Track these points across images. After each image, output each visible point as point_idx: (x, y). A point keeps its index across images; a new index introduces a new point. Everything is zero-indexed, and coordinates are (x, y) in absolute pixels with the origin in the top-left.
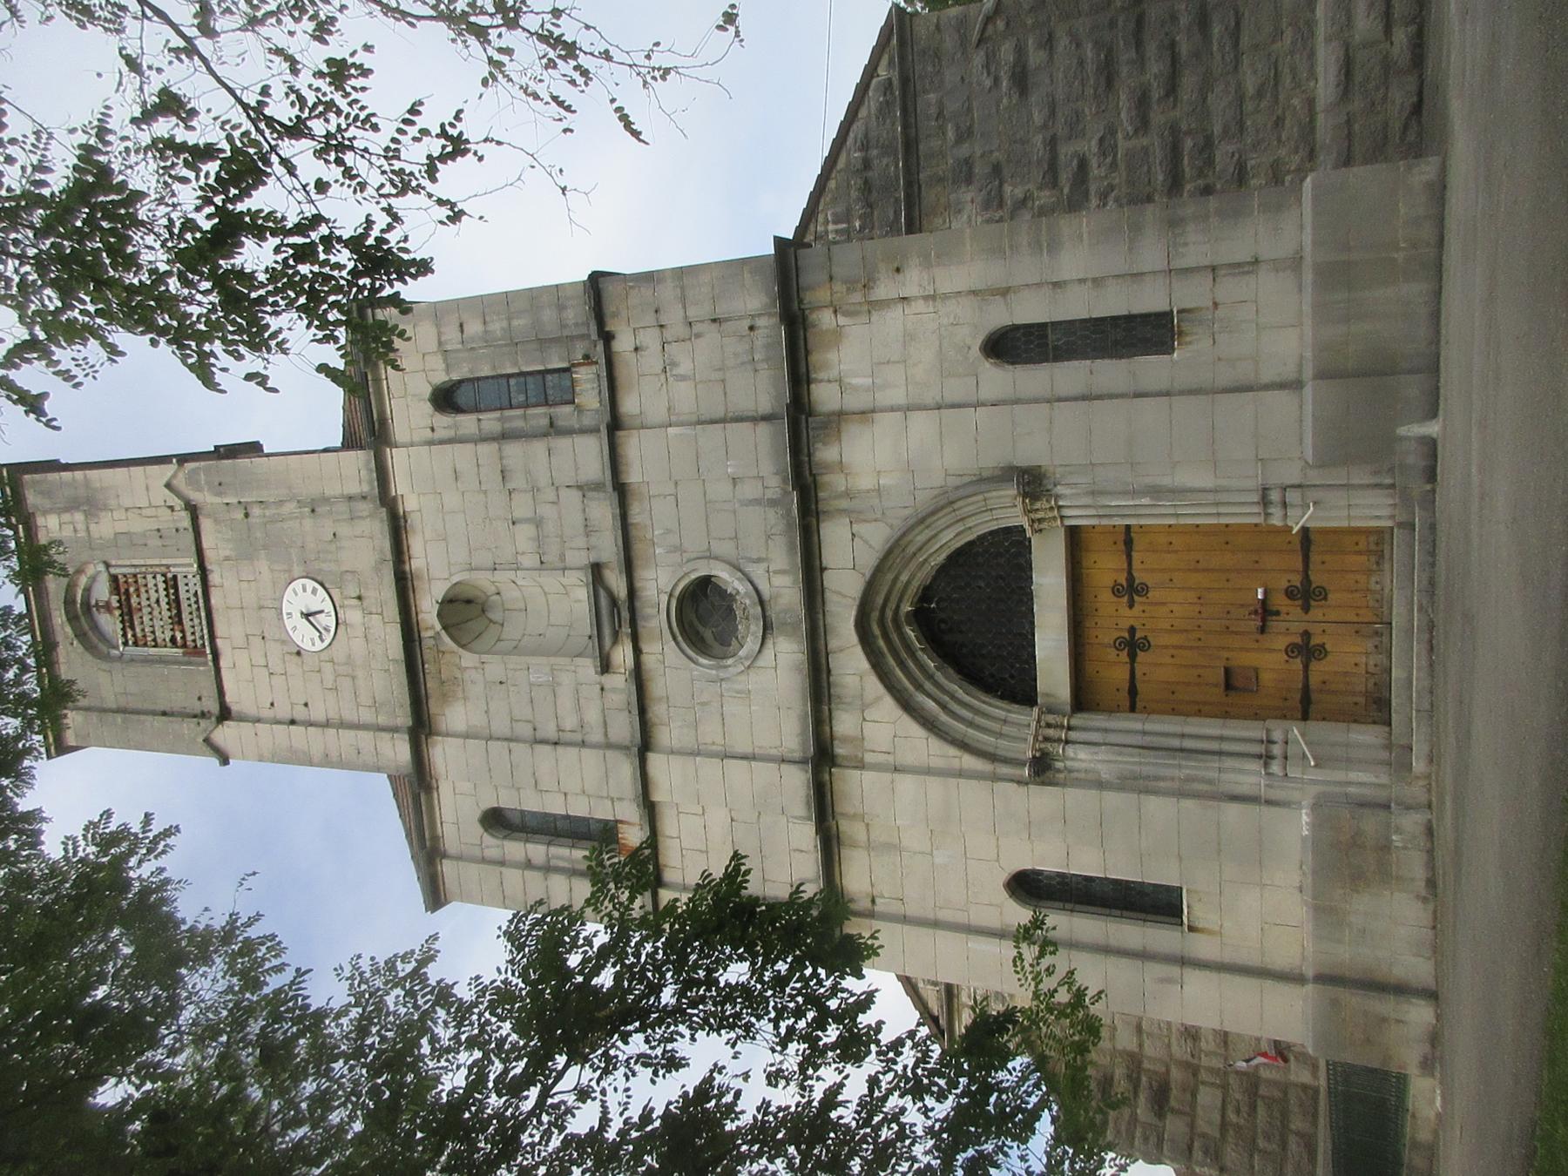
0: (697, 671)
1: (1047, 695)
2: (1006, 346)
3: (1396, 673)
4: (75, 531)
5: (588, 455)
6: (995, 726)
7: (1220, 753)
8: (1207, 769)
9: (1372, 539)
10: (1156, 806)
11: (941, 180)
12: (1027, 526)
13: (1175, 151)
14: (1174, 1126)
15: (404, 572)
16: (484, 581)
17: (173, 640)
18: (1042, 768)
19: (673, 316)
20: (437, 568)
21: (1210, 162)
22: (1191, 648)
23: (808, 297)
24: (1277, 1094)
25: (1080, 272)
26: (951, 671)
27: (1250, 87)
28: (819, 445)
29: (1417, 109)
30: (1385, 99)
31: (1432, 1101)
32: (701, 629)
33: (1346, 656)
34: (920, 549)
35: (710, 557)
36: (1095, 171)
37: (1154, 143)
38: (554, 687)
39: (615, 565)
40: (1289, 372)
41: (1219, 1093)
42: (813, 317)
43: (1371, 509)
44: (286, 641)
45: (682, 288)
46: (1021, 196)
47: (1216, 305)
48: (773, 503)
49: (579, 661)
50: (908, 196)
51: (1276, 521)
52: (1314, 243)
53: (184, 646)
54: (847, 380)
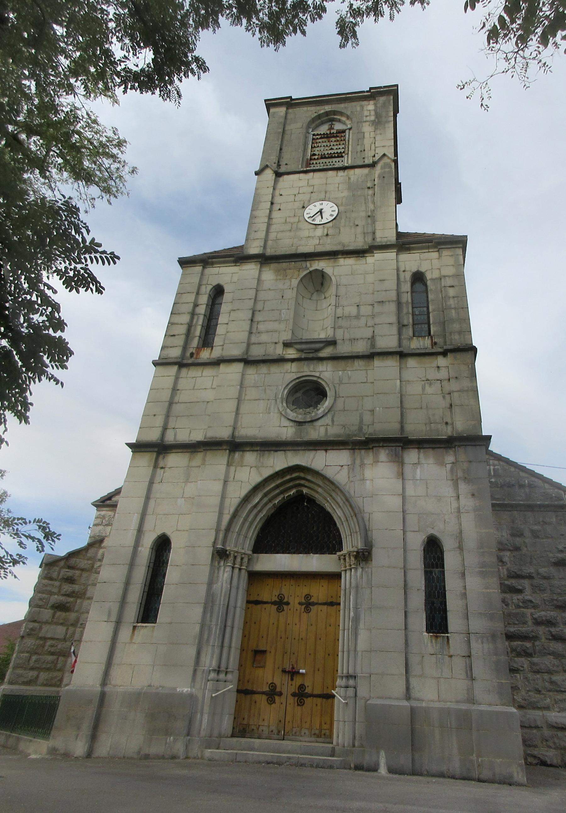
0: (281, 389)
1: (258, 559)
2: (433, 549)
3: (257, 742)
4: (366, 116)
5: (388, 340)
6: (244, 532)
7: (222, 646)
8: (215, 640)
9: (328, 732)
10: (196, 613)
11: (513, 522)
12: (342, 553)
13: (524, 637)
14: (47, 614)
15: (338, 255)
16: (332, 291)
17: (314, 155)
18: (221, 554)
19: (454, 386)
20: (339, 270)
21: (519, 655)
22: (277, 633)
23: (461, 451)
24: (59, 666)
25: (469, 588)
26: (273, 511)
27: (555, 678)
28: (387, 451)
29: (543, 763)
30: (550, 747)
31: (36, 753)
32: (302, 391)
33: (268, 715)
34: (334, 499)
35: (336, 397)
36: (516, 597)
37: (528, 628)
38: (279, 321)
39: (335, 351)
40: (415, 693)
41: (62, 637)
42: (451, 452)
43: (342, 734)
44: (310, 202)
45: (467, 391)
46: (504, 560)
47: (451, 656)
48: (360, 429)
49: (290, 333)
50: (506, 505)
51: (339, 682)
52: (481, 711)
53: (311, 159)
54: (419, 467)
